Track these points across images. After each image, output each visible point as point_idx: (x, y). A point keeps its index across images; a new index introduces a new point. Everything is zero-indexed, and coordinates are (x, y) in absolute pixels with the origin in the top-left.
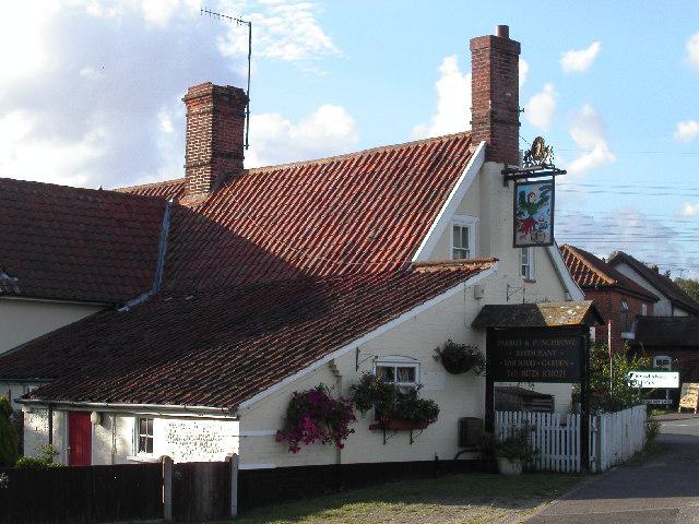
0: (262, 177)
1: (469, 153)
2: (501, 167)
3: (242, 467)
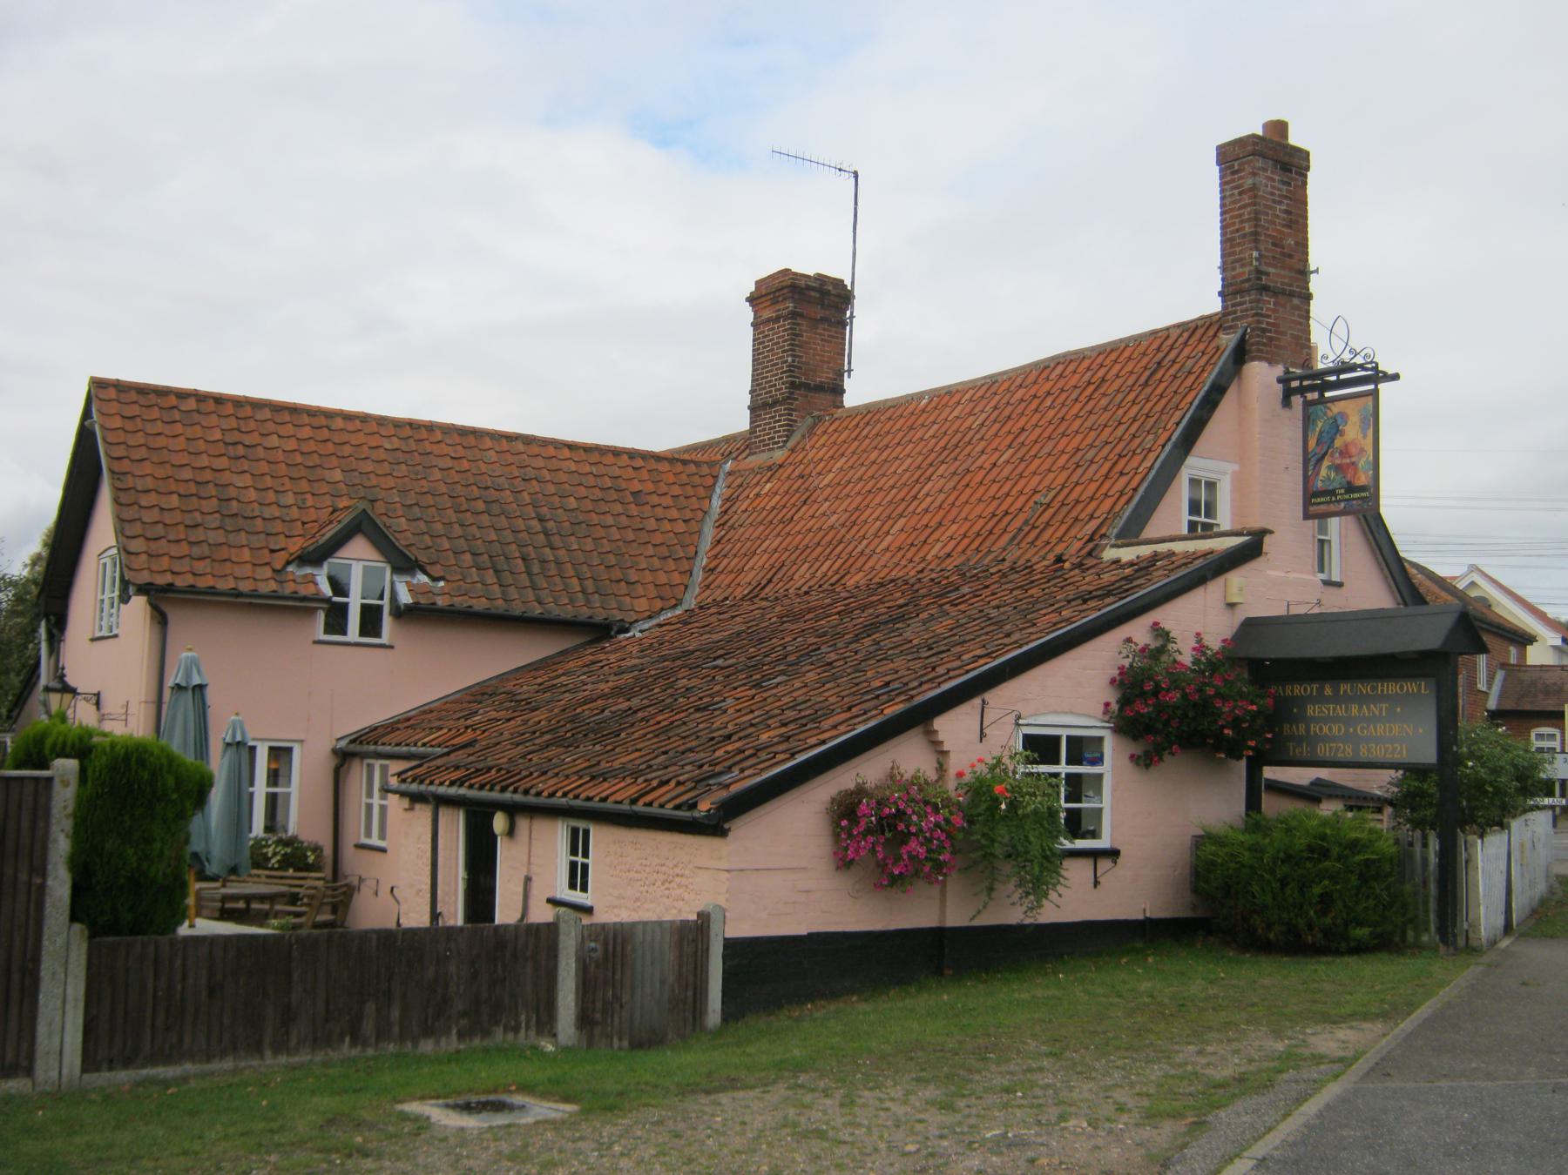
0: (872, 412)
1: (1218, 348)
2: (1279, 370)
3: (731, 933)
